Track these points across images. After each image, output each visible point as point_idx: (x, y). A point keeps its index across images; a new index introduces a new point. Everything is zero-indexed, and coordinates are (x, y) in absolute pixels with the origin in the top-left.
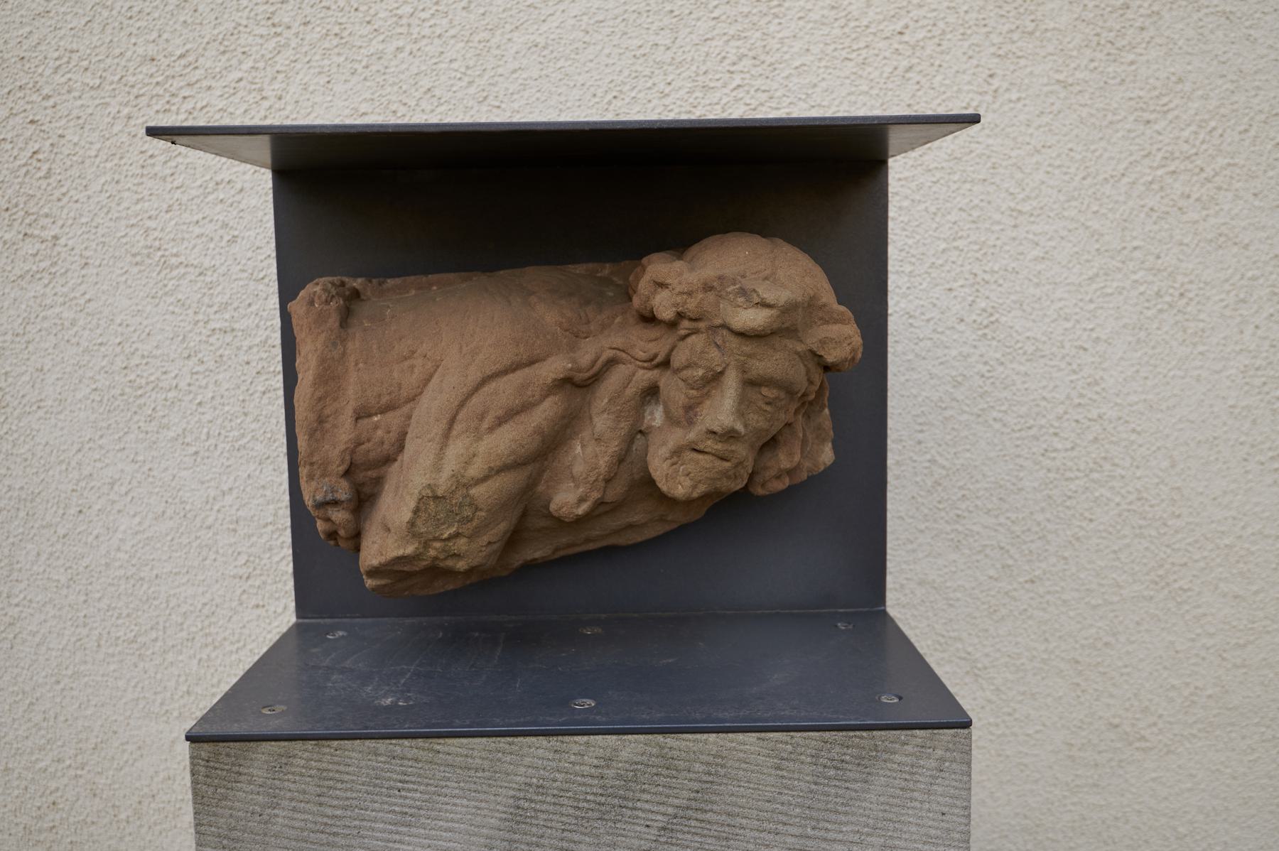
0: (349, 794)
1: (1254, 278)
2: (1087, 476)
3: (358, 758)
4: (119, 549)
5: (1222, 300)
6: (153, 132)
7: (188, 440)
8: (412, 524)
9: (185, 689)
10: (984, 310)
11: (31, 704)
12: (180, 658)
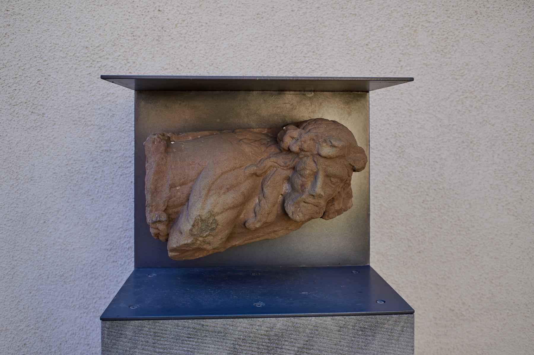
0: (166, 343)
1: (497, 137)
2: (439, 211)
3: (170, 326)
4: (59, 238)
5: (486, 145)
6: (103, 77)
7: (90, 194)
8: (191, 230)
9: (82, 296)
10: (400, 147)
11: (19, 302)
12: (81, 283)
